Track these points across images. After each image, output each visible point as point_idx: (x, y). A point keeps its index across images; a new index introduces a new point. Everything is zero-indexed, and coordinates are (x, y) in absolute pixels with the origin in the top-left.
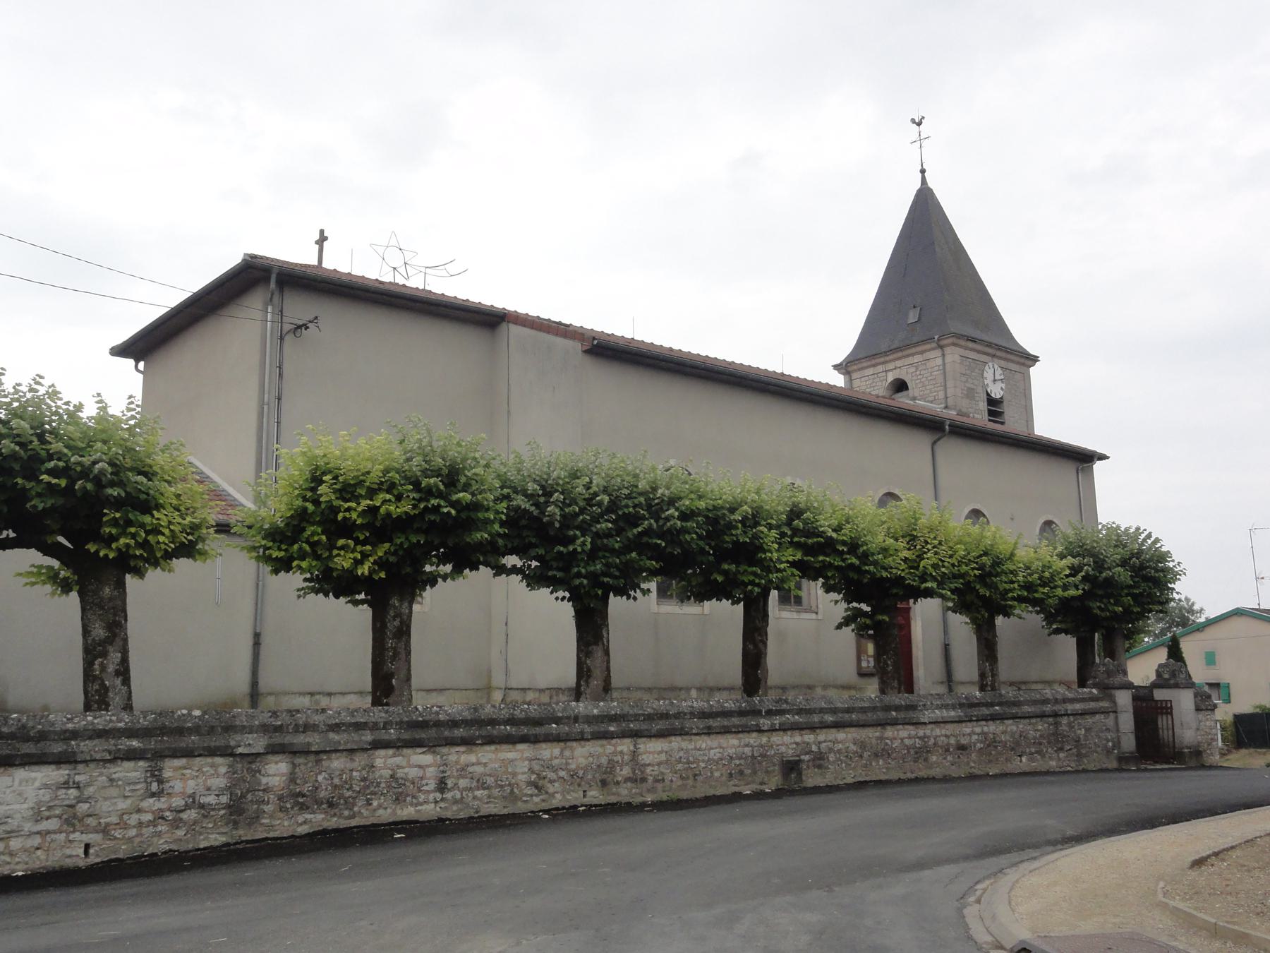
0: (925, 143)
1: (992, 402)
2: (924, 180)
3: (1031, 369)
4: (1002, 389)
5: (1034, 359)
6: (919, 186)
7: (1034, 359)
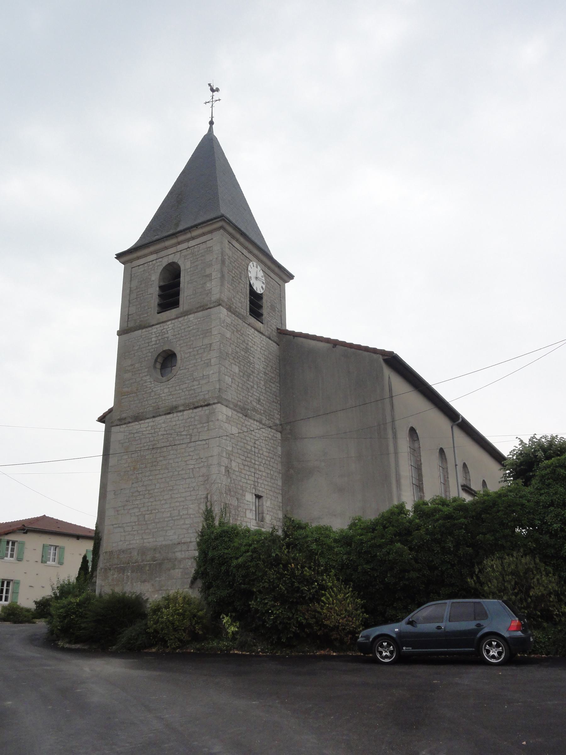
0: (215, 104)
1: (253, 294)
2: (211, 130)
3: (286, 284)
4: (262, 287)
5: (291, 277)
6: (206, 132)
7: (291, 277)
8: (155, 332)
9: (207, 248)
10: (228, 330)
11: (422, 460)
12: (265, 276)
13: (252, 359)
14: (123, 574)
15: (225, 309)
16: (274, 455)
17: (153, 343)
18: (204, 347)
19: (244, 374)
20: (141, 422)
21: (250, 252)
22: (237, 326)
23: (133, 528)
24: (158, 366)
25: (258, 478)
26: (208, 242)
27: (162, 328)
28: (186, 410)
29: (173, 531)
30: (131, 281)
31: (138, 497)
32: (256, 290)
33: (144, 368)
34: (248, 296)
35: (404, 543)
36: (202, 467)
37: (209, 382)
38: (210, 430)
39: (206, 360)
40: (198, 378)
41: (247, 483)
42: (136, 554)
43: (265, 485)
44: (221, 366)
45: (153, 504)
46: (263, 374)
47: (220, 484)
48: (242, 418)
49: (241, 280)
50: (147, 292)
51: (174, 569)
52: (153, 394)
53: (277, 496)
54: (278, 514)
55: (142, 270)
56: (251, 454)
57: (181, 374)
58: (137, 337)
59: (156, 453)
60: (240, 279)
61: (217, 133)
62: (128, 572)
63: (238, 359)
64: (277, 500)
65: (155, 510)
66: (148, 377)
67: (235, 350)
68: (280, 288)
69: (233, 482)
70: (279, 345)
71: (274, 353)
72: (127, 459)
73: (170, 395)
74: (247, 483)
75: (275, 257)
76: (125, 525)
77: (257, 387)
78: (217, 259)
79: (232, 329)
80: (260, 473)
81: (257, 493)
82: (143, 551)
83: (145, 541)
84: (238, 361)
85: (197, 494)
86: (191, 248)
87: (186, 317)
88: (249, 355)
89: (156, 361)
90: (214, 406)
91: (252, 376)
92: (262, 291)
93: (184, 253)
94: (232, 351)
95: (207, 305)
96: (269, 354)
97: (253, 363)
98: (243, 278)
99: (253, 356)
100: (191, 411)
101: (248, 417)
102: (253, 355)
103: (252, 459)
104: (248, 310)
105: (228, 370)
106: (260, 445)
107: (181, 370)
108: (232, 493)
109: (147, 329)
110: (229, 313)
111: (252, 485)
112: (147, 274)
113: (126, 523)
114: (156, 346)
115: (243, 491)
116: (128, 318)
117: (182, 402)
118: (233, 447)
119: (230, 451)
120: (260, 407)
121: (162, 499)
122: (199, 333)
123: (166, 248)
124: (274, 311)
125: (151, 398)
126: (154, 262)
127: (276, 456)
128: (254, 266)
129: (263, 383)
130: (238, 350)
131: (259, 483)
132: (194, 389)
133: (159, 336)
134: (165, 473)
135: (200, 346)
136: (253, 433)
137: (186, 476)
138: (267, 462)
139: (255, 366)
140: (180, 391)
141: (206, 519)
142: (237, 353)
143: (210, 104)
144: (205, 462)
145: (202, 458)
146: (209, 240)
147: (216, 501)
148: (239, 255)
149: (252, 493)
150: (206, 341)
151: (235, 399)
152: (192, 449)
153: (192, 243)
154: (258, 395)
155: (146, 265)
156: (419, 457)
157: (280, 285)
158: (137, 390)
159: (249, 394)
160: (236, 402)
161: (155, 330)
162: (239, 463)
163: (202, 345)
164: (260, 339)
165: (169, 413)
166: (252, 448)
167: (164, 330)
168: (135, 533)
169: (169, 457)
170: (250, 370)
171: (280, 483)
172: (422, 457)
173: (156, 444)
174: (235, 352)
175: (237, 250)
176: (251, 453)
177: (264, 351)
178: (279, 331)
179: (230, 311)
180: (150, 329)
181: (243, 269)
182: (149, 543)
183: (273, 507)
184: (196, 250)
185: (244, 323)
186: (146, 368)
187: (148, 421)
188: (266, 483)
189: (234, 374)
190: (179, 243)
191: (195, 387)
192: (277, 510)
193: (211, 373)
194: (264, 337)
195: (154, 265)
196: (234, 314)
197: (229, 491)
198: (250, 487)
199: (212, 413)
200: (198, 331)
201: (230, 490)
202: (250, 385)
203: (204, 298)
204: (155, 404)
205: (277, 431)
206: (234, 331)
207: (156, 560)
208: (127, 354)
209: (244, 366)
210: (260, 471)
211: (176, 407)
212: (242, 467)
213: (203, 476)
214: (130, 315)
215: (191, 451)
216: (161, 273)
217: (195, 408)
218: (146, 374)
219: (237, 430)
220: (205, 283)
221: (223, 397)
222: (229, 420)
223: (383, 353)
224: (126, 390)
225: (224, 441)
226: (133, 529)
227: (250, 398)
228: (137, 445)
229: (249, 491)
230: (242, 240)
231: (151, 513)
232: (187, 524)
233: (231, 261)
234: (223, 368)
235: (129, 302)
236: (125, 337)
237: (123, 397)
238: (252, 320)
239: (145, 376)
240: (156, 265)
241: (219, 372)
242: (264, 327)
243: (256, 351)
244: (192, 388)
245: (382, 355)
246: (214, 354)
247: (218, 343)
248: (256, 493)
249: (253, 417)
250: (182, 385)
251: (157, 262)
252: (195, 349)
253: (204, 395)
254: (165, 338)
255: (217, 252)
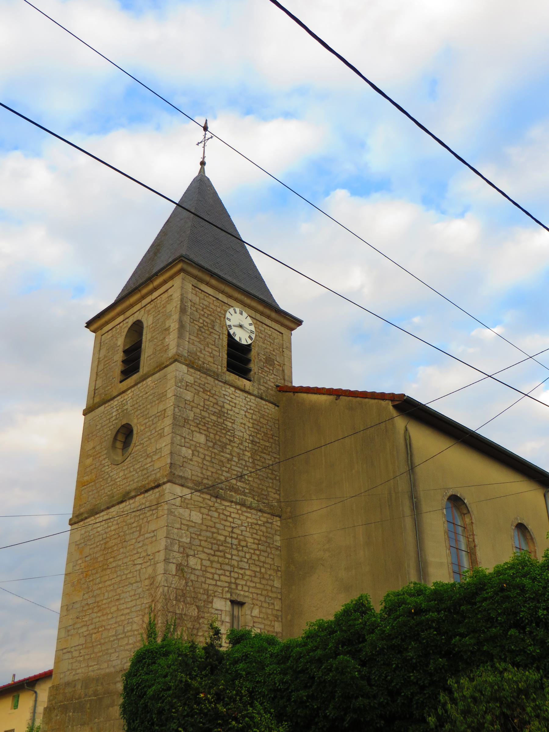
2: (202, 171)
7: (299, 322)
8: (116, 405)
9: (168, 297)
10: (188, 390)
11: (476, 540)
12: (255, 324)
13: (230, 424)
14: (66, 715)
15: (184, 366)
16: (269, 547)
17: (114, 418)
18: (159, 414)
19: (215, 444)
20: (96, 516)
21: (230, 297)
22: (204, 385)
23: (80, 653)
24: (119, 445)
25: (236, 579)
26: (169, 290)
27: (122, 399)
28: (138, 495)
29: (117, 654)
30: (100, 351)
31: (88, 611)
32: (238, 341)
33: (104, 449)
34: (226, 348)
35: (354, 654)
36: (148, 566)
37: (161, 457)
38: (158, 518)
39: (160, 430)
40: (151, 454)
41: (216, 585)
42: (79, 687)
43: (249, 587)
44: (174, 435)
45: (100, 619)
46: (248, 443)
47: (166, 588)
48: (210, 500)
49: (214, 330)
50: (113, 360)
51: (112, 707)
52: (109, 479)
53: (272, 601)
54: (274, 626)
55: (110, 335)
56: (224, 546)
57: (136, 451)
58: (100, 414)
59: (108, 553)
60: (213, 328)
61: (209, 173)
62: (70, 712)
63: (205, 426)
64: (271, 607)
65: (101, 627)
66: (107, 460)
67: (201, 414)
68: (282, 337)
69: (190, 584)
70: (278, 406)
71: (270, 416)
72: (80, 564)
73: (124, 479)
74: (216, 585)
75: (283, 306)
76: (72, 650)
77: (239, 460)
78: (176, 307)
79: (195, 389)
80: (241, 572)
81: (235, 598)
82: (87, 682)
83: (91, 668)
84: (205, 428)
85: (142, 602)
86: (154, 301)
87: (144, 382)
88: (224, 420)
89: (115, 439)
90: (164, 486)
91: (228, 447)
92: (250, 342)
93: (149, 307)
94: (195, 416)
95: (163, 364)
96: (260, 417)
97: (232, 430)
98: (217, 328)
99: (233, 421)
100: (142, 496)
101: (220, 498)
102: (233, 420)
103: (227, 553)
104: (225, 365)
105: (187, 440)
106: (242, 535)
107: (137, 446)
108: (188, 599)
109: (109, 404)
110: (192, 370)
111: (226, 587)
112: (114, 339)
113: (75, 646)
114: (116, 421)
115: (208, 596)
116: (95, 393)
117: (134, 486)
118: (191, 538)
119: (187, 543)
120: (244, 486)
121: (109, 612)
122: (155, 399)
123: (132, 306)
124: (273, 365)
125: (108, 485)
126: (121, 324)
127: (271, 548)
128: (236, 313)
129: (248, 454)
130: (206, 415)
131: (239, 584)
132: (147, 469)
133: (120, 409)
134: (114, 578)
135: (155, 414)
136: (230, 519)
137: (133, 580)
138: (255, 557)
139: (236, 433)
140: (134, 473)
141: (149, 636)
142: (204, 418)
143: (202, 145)
144: (152, 559)
145: (149, 555)
146: (171, 288)
147: (160, 611)
148: (211, 301)
149: (226, 599)
150: (161, 407)
151: (198, 476)
152: (140, 544)
153: (156, 294)
154: (240, 470)
155: (114, 329)
156: (472, 537)
157: (282, 334)
158: (96, 477)
159: (224, 469)
160: (200, 479)
161: (116, 403)
162: (202, 560)
163: (158, 413)
164: (245, 399)
165: (122, 502)
166: (228, 538)
167: (124, 402)
168: (81, 659)
169: (119, 557)
170: (227, 438)
171: (277, 584)
172: (475, 537)
173: (108, 542)
174: (201, 418)
175: (208, 295)
176: (224, 545)
177: (252, 414)
178: (278, 389)
179: (192, 367)
180: (112, 402)
181: (218, 317)
182: (93, 671)
183: (265, 617)
184: (158, 302)
185: (217, 382)
186: (105, 450)
187: (102, 514)
188: (252, 585)
189: (198, 445)
190: (143, 297)
191: (148, 466)
192: (271, 621)
193: (163, 445)
194: (253, 398)
195: (121, 327)
196: (199, 371)
197: (181, 596)
198: (223, 590)
199: (162, 495)
200: (154, 397)
201: (184, 595)
202: (226, 458)
203: (162, 357)
204: (111, 492)
205: (274, 515)
206: (199, 391)
207: (98, 695)
208: (91, 435)
209: (215, 435)
210: (241, 569)
211: (128, 493)
212: (207, 563)
213: (149, 578)
214: (97, 389)
215: (140, 547)
216: (126, 335)
217: (147, 491)
218: (105, 457)
219: (201, 516)
220: (165, 338)
221: (177, 473)
222: (185, 503)
223: (392, 397)
224: (86, 478)
225: (176, 531)
226: (81, 654)
227: (225, 474)
228: (91, 545)
229: (221, 596)
230: (214, 282)
231: (98, 632)
232: (130, 644)
233: (197, 309)
234: (179, 438)
235: (97, 375)
236: (90, 416)
237: (83, 488)
238: (232, 377)
239: (104, 459)
240: (123, 327)
241: (172, 443)
242: (253, 386)
243: (237, 415)
244: (145, 467)
245: (392, 401)
246: (168, 421)
247: (172, 407)
248: (232, 599)
249: (228, 498)
250: (136, 464)
251: (123, 324)
252: (151, 419)
253: (156, 474)
254: (124, 410)
255: (177, 299)
